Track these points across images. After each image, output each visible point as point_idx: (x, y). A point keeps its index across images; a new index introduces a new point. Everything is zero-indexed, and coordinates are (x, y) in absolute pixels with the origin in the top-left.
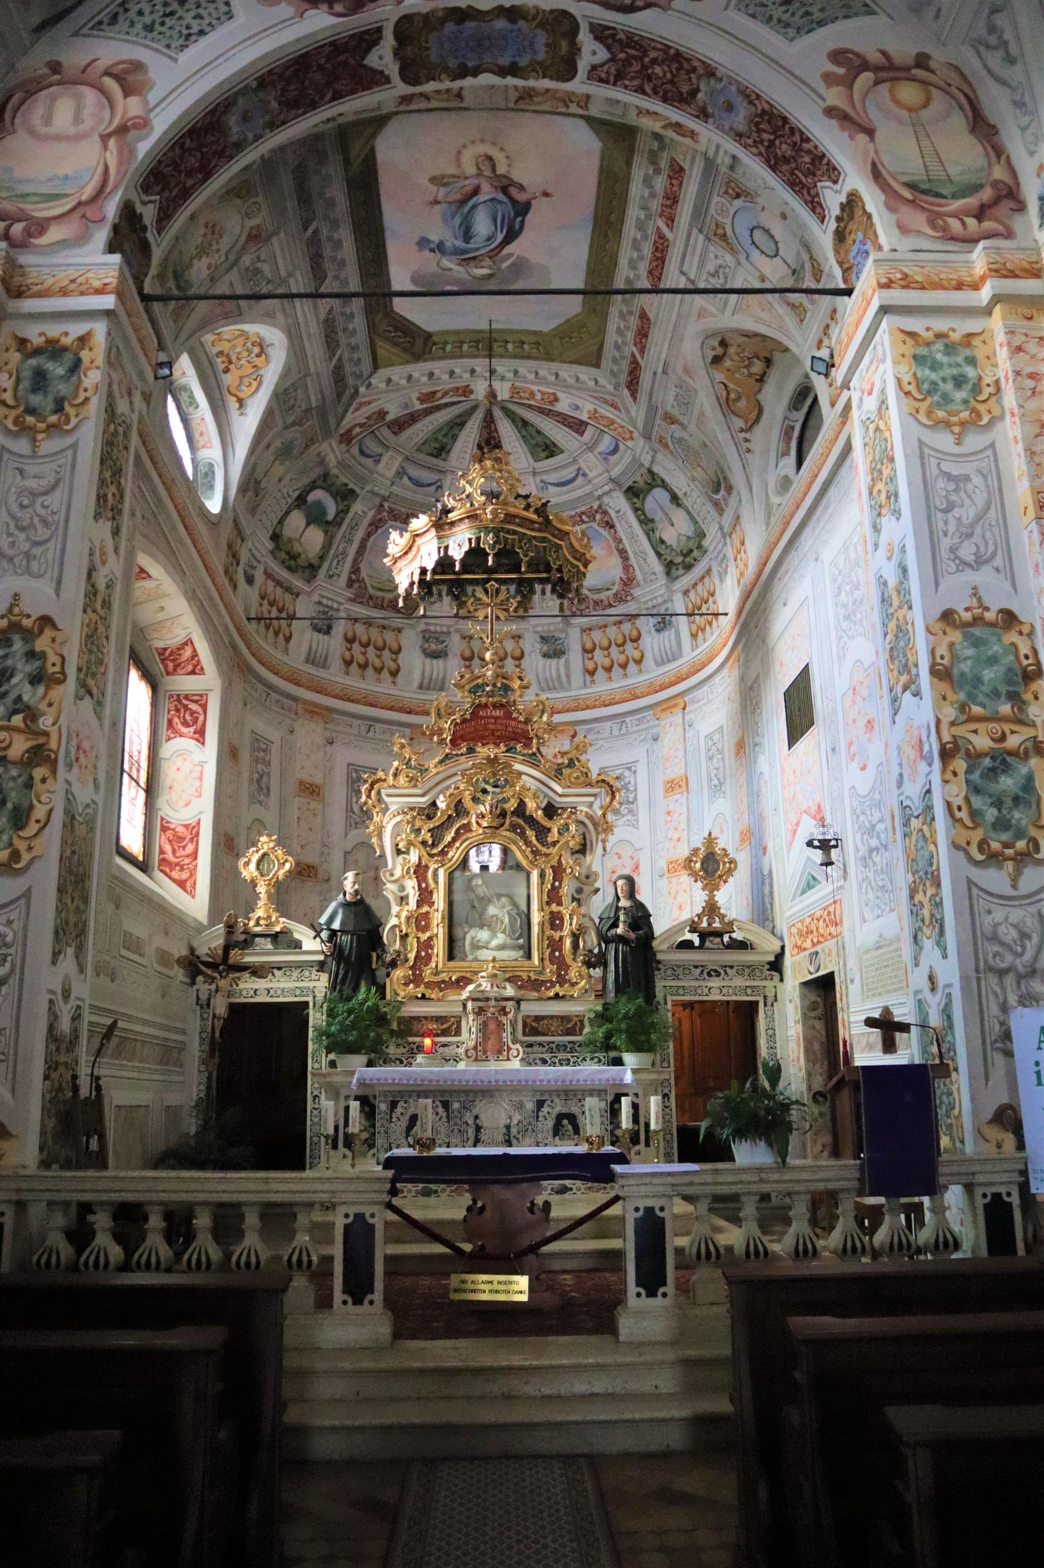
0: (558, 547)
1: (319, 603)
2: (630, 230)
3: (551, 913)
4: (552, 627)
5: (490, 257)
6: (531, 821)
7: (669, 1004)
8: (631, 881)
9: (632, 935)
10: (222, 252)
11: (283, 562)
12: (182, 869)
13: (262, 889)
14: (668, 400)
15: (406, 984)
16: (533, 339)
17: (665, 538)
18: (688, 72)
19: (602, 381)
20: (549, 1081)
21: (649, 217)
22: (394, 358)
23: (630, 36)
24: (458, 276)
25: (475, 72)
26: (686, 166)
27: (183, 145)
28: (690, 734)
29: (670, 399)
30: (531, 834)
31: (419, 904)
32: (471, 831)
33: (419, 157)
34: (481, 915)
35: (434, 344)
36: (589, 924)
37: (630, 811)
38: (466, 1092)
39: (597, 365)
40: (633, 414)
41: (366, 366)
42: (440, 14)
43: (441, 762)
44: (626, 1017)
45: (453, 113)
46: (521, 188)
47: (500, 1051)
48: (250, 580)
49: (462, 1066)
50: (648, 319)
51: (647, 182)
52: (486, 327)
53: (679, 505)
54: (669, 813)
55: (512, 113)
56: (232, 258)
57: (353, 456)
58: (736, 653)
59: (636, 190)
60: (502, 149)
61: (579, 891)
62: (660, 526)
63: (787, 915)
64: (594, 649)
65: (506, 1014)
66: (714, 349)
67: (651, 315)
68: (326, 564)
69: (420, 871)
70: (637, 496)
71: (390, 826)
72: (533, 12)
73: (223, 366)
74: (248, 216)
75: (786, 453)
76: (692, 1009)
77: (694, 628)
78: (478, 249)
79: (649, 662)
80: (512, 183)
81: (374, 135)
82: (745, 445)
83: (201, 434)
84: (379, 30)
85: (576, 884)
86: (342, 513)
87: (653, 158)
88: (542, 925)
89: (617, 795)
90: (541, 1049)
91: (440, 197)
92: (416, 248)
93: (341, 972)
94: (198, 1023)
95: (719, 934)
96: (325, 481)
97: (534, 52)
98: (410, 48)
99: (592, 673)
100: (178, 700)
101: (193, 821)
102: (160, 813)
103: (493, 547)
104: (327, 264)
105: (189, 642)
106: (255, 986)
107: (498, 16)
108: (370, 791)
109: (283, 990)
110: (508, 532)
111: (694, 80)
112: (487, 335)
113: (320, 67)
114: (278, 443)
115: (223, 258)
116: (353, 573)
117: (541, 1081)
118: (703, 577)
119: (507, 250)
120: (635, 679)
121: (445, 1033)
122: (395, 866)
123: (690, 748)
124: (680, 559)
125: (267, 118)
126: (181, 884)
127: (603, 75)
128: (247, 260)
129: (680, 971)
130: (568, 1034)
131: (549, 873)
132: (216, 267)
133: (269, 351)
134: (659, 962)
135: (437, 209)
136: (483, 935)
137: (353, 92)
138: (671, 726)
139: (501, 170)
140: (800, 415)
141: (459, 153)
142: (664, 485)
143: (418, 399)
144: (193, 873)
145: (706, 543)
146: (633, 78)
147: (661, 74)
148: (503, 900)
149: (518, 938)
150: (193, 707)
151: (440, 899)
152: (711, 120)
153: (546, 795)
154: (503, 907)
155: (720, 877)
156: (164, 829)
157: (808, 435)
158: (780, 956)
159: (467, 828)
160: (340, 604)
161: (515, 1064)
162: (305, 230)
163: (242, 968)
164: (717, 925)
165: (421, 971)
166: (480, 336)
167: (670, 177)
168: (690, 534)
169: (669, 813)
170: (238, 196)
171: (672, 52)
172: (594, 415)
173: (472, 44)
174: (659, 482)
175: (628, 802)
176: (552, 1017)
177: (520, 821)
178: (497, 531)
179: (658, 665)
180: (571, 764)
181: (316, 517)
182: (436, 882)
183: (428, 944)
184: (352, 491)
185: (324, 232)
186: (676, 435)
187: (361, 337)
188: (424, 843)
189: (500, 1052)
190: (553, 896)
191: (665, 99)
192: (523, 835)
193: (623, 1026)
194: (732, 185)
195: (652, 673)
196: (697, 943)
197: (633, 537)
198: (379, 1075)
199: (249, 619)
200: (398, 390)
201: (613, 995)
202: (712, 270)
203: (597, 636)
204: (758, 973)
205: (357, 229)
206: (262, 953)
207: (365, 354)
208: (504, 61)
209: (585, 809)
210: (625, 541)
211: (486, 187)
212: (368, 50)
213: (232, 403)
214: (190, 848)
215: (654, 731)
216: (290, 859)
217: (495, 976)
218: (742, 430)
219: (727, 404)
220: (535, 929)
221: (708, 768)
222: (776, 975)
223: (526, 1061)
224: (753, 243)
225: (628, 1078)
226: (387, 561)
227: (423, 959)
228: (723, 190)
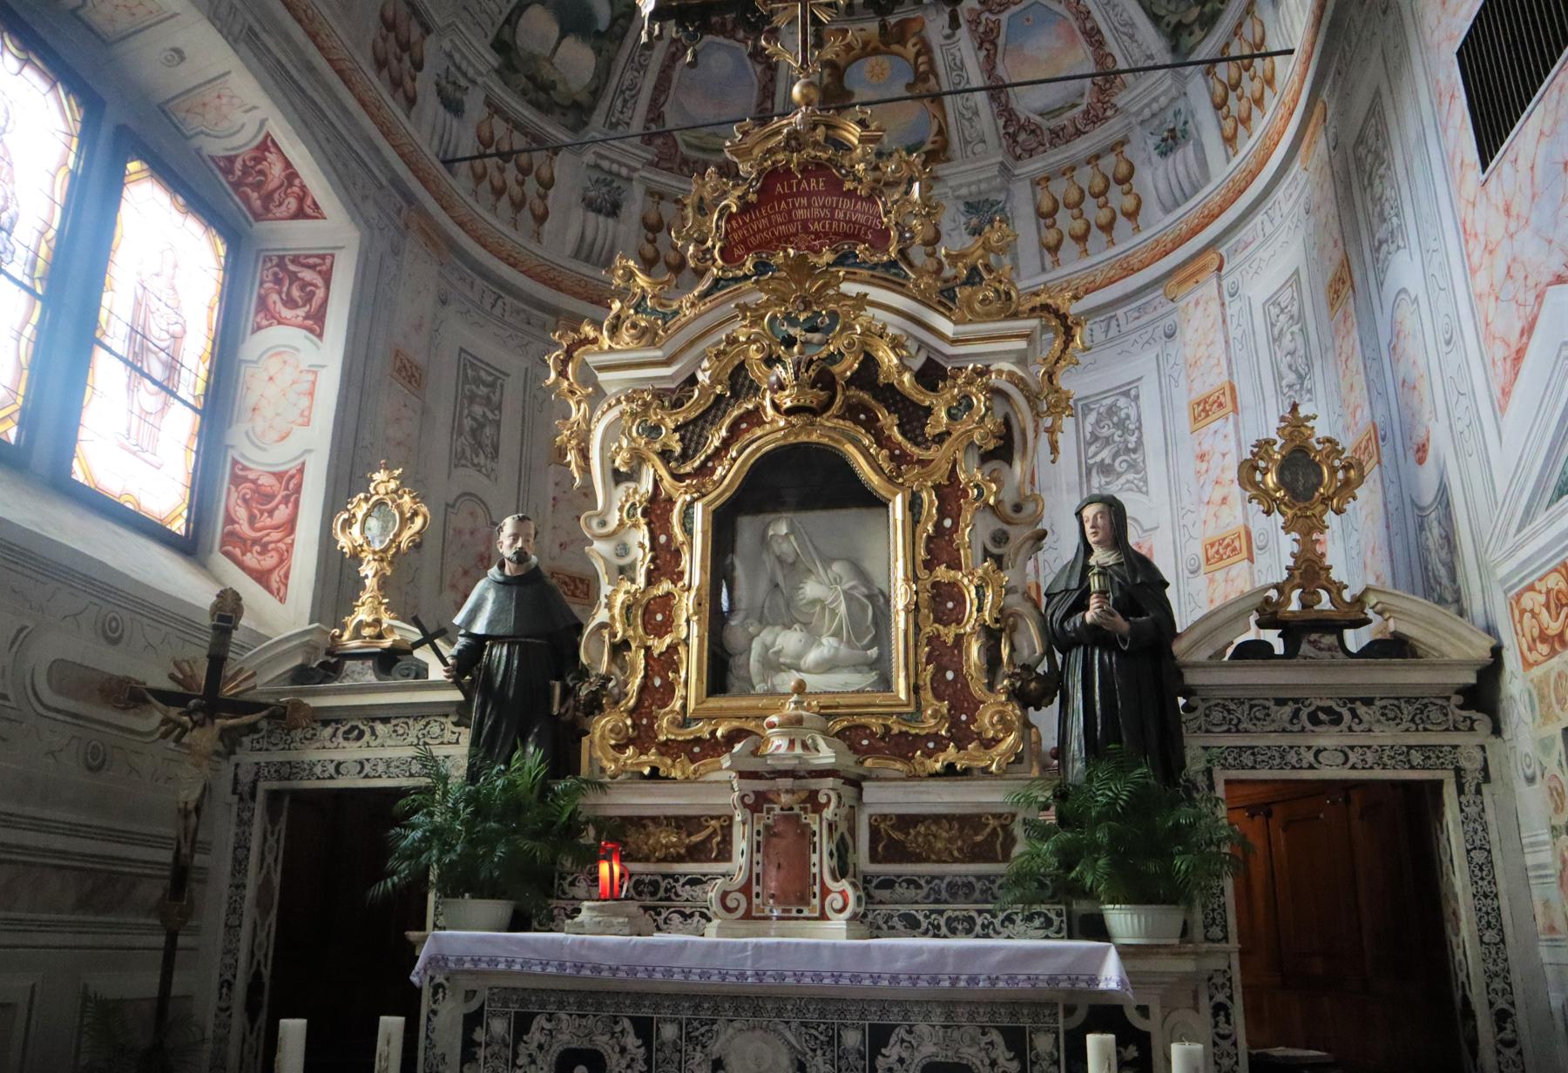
1: (597, 166)
3: (935, 585)
4: (983, 186)
6: (891, 396)
7: (1220, 791)
8: (1115, 513)
9: (1121, 624)
11: (524, 93)
12: (265, 550)
13: (368, 570)
15: (620, 748)
20: (894, 978)
28: (1233, 308)
30: (889, 421)
31: (651, 580)
32: (761, 423)
34: (789, 603)
36: (1025, 608)
37: (1132, 466)
38: (697, 999)
43: (705, 295)
44: (1108, 813)
47: (799, 896)
49: (712, 934)
54: (1202, 457)
58: (1318, 111)
61: (1000, 538)
63: (1502, 571)
64: (1055, 209)
65: (818, 808)
68: (604, 105)
69: (656, 510)
71: (601, 432)
76: (1269, 815)
77: (1229, 125)
79: (1151, 208)
85: (990, 524)
88: (914, 610)
89: (1078, 331)
90: (912, 893)
93: (488, 723)
94: (233, 829)
95: (1334, 626)
99: (1054, 249)
100: (281, 262)
101: (292, 467)
102: (232, 453)
105: (267, 145)
106: (338, 756)
108: (565, 363)
109: (388, 763)
116: (652, 120)
117: (876, 978)
118: (1240, 25)
120: (1128, 241)
121: (695, 853)
122: (613, 505)
123: (1235, 333)
126: (261, 577)
129: (1241, 712)
130: (973, 859)
131: (929, 498)
134: (1188, 692)
136: (788, 641)
138: (1198, 312)
144: (284, 557)
148: (837, 568)
149: (869, 647)
150: (307, 275)
151: (694, 565)
153: (922, 345)
154: (838, 580)
155: (1326, 500)
156: (237, 480)
158: (1492, 670)
159: (754, 417)
160: (635, 170)
161: (835, 931)
163: (327, 718)
164: (1325, 602)
165: (653, 719)
169: (1202, 457)
175: (1128, 451)
176: (937, 819)
177: (865, 396)
179: (1167, 211)
180: (974, 277)
182: (688, 531)
183: (669, 661)
188: (665, 455)
189: (804, 899)
190: (938, 549)
192: (871, 425)
193: (1101, 836)
195: (1157, 223)
196: (1279, 648)
198: (480, 951)
199: (448, 163)
201: (1079, 765)
203: (1059, 187)
204: (1435, 715)
206: (360, 688)
209: (1006, 366)
210: (1097, 15)
214: (282, 513)
215: (1168, 321)
216: (424, 509)
217: (799, 721)
220: (900, 621)
221: (1273, 355)
222: (1483, 722)
223: (865, 923)
225: (1111, 974)
227: (655, 694)
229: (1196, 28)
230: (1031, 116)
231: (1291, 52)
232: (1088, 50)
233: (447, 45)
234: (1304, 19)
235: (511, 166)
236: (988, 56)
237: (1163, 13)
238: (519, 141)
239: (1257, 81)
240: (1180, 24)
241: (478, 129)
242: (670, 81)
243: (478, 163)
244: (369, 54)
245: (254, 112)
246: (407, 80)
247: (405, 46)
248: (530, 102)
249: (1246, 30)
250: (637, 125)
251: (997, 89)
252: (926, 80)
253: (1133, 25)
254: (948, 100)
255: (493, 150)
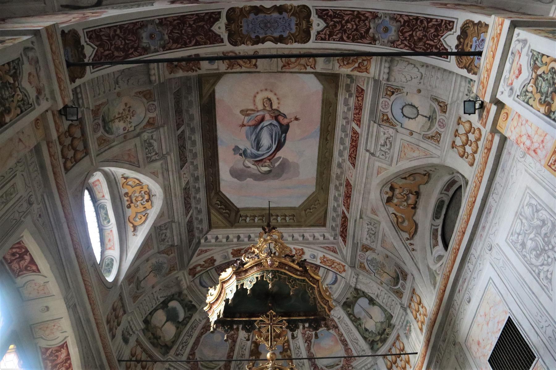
0: (313, 288)
2: (338, 133)
5: (270, 160)
10: (133, 125)
11: (150, 339)
14: (364, 238)
16: (292, 212)
17: (367, 327)
18: (364, 21)
19: (327, 235)
21: (348, 123)
22: (220, 223)
23: (335, 12)
24: (254, 172)
25: (263, 41)
26: (365, 88)
27: (115, 31)
29: (365, 235)
33: (236, 96)
35: (241, 216)
39: (324, 225)
40: (345, 253)
41: (205, 226)
42: (247, 9)
45: (253, 75)
46: (285, 116)
48: (126, 341)
50: (351, 186)
51: (346, 103)
52: (266, 206)
53: (374, 304)
55: (280, 74)
56: (138, 130)
57: (196, 285)
59: (341, 108)
60: (275, 94)
62: (364, 321)
66: (387, 193)
67: (352, 183)
68: (175, 347)
70: (349, 306)
72: (290, 8)
73: (127, 203)
74: (148, 110)
75: (436, 245)
78: (263, 155)
80: (280, 114)
81: (215, 83)
82: (411, 247)
83: (110, 240)
84: (219, 13)
86: (188, 318)
87: (348, 88)
91: (245, 123)
92: (232, 152)
96: (179, 296)
97: (291, 29)
98: (233, 26)
103: (272, 280)
104: (188, 154)
107: (273, 12)
110: (281, 273)
111: (367, 24)
112: (268, 212)
113: (190, 26)
114: (154, 261)
115: (133, 128)
116: (191, 355)
118: (395, 343)
119: (279, 154)
124: (378, 338)
125: (162, 42)
127: (323, 36)
128: (145, 136)
132: (128, 132)
133: (153, 199)
135: (244, 129)
137: (205, 43)
139: (275, 107)
140: (440, 222)
141: (255, 96)
142: (365, 295)
143: (232, 253)
145: (393, 321)
146: (338, 34)
147: (351, 27)
152: (377, 42)
157: (447, 229)
162: (178, 129)
166: (264, 212)
167: (357, 97)
168: (382, 320)
170: (145, 96)
171: (356, 13)
172: (324, 260)
173: (262, 25)
174: (361, 293)
178: (274, 272)
181: (172, 317)
184: (194, 306)
185: (187, 133)
186: (369, 258)
187: (203, 205)
191: (353, 41)
194: (389, 89)
197: (349, 332)
199: (119, 361)
200: (220, 246)
202: (383, 142)
205: (203, 136)
207: (204, 216)
208: (276, 35)
210: (345, 335)
211: (267, 117)
212: (213, 23)
213: (130, 227)
218: (408, 239)
219: (398, 226)
224: (404, 115)
226: (206, 309)
228: (384, 94)
229: (379, 343)
230: (323, 367)
231: (417, 353)
232: (343, 346)
233: (129, 318)
234: (421, 345)
235: (139, 365)
236: (308, 345)
237: (367, 337)
238: (144, 357)
239: (403, 361)
240: (373, 341)
241: (132, 349)
242: (199, 341)
243: (128, 363)
244: (106, 316)
245: (64, 333)
246: (114, 329)
247: (117, 317)
248: (151, 343)
249: (397, 344)
250: (184, 358)
251: (311, 358)
252: (287, 351)
253: (357, 340)
254: (294, 361)
255: (134, 359)
